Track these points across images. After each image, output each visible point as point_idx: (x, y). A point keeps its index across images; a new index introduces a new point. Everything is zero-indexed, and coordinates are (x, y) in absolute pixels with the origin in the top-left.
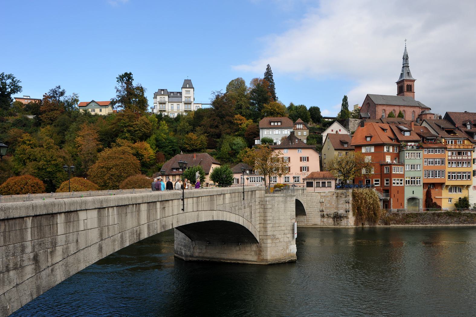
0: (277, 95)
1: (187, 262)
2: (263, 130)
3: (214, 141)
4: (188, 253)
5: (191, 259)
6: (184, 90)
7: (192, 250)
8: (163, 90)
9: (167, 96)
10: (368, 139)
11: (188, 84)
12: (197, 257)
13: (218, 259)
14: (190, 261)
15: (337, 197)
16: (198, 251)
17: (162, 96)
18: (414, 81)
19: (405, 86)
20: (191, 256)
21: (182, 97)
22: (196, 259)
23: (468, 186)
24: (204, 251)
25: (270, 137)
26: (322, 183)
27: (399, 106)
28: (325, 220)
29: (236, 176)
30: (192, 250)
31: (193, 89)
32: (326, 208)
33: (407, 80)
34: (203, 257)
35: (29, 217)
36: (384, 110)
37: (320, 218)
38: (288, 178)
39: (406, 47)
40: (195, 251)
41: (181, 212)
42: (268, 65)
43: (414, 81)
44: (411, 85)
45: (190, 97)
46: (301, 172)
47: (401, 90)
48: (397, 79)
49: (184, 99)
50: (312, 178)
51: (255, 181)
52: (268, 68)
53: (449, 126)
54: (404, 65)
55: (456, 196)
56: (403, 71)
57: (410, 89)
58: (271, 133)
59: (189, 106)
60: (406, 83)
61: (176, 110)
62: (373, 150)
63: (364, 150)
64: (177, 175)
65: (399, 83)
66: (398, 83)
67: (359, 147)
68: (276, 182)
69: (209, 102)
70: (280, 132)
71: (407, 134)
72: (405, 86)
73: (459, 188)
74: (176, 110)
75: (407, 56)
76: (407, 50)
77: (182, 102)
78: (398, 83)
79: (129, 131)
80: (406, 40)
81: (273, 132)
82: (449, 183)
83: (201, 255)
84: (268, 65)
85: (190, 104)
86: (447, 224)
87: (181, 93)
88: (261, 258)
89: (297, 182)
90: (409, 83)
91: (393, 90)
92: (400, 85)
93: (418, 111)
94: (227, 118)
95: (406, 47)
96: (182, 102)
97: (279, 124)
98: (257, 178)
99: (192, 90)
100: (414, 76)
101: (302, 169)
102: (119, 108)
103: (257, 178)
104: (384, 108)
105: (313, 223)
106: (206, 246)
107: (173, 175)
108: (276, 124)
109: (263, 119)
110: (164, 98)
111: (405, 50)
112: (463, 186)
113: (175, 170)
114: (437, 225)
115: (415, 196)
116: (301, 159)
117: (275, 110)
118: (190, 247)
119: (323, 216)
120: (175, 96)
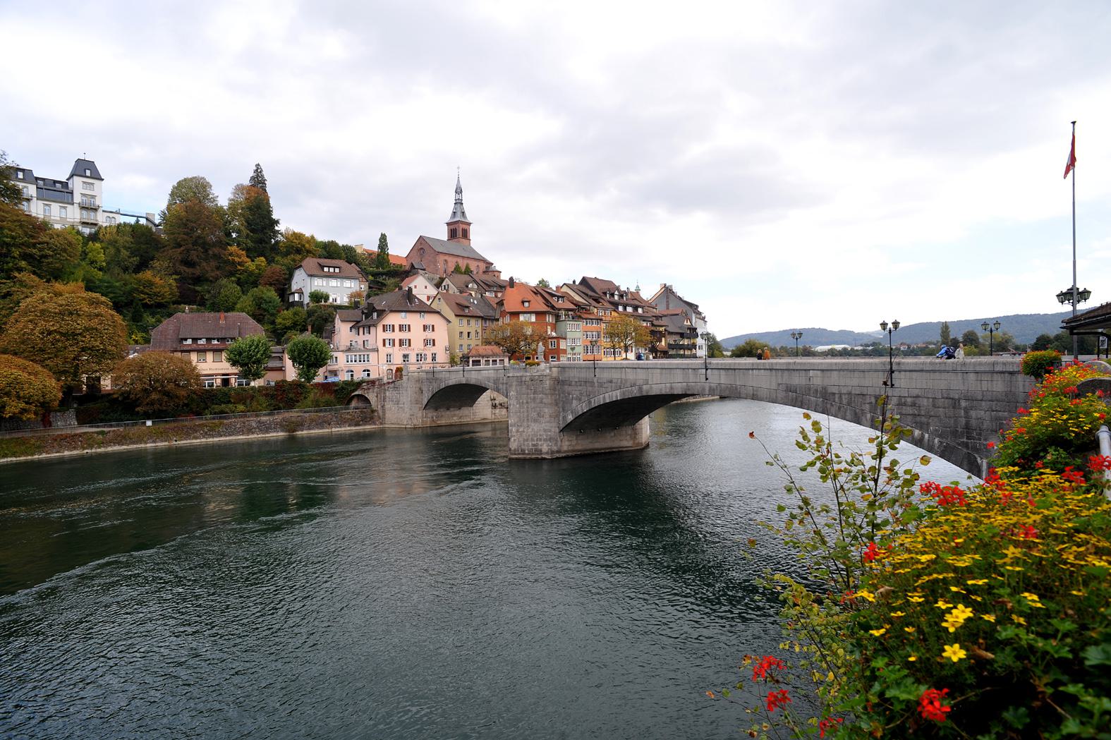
0: (1099, 305)
1: (552, 459)
3: (189, 289)
4: (555, 448)
5: (558, 455)
7: (559, 443)
9: (35, 186)
10: (526, 304)
12: (565, 452)
13: (590, 450)
14: (557, 458)
16: (567, 443)
18: (469, 224)
19: (459, 230)
20: (558, 452)
22: (564, 455)
24: (574, 443)
25: (324, 290)
27: (463, 257)
28: (497, 411)
30: (559, 443)
34: (573, 451)
36: (446, 261)
37: (490, 409)
40: (563, 444)
42: (258, 165)
43: (469, 224)
47: (453, 234)
48: (448, 218)
49: (77, 198)
50: (479, 356)
52: (257, 170)
56: (455, 208)
57: (465, 234)
59: (92, 214)
61: (58, 219)
62: (533, 318)
63: (522, 318)
66: (448, 224)
67: (515, 314)
70: (339, 283)
72: (459, 230)
74: (58, 219)
77: (73, 204)
79: (25, 257)
80: (458, 168)
81: (328, 284)
83: (570, 448)
84: (258, 165)
85: (95, 210)
86: (267, 432)
88: (637, 442)
92: (452, 227)
94: (216, 250)
96: (73, 204)
97: (337, 270)
98: (360, 355)
101: (426, 342)
103: (360, 355)
104: (446, 258)
105: (482, 417)
106: (577, 436)
107: (199, 351)
108: (332, 270)
111: (458, 181)
113: (216, 342)
114: (93, 450)
116: (425, 328)
117: (304, 246)
118: (557, 441)
119: (494, 406)
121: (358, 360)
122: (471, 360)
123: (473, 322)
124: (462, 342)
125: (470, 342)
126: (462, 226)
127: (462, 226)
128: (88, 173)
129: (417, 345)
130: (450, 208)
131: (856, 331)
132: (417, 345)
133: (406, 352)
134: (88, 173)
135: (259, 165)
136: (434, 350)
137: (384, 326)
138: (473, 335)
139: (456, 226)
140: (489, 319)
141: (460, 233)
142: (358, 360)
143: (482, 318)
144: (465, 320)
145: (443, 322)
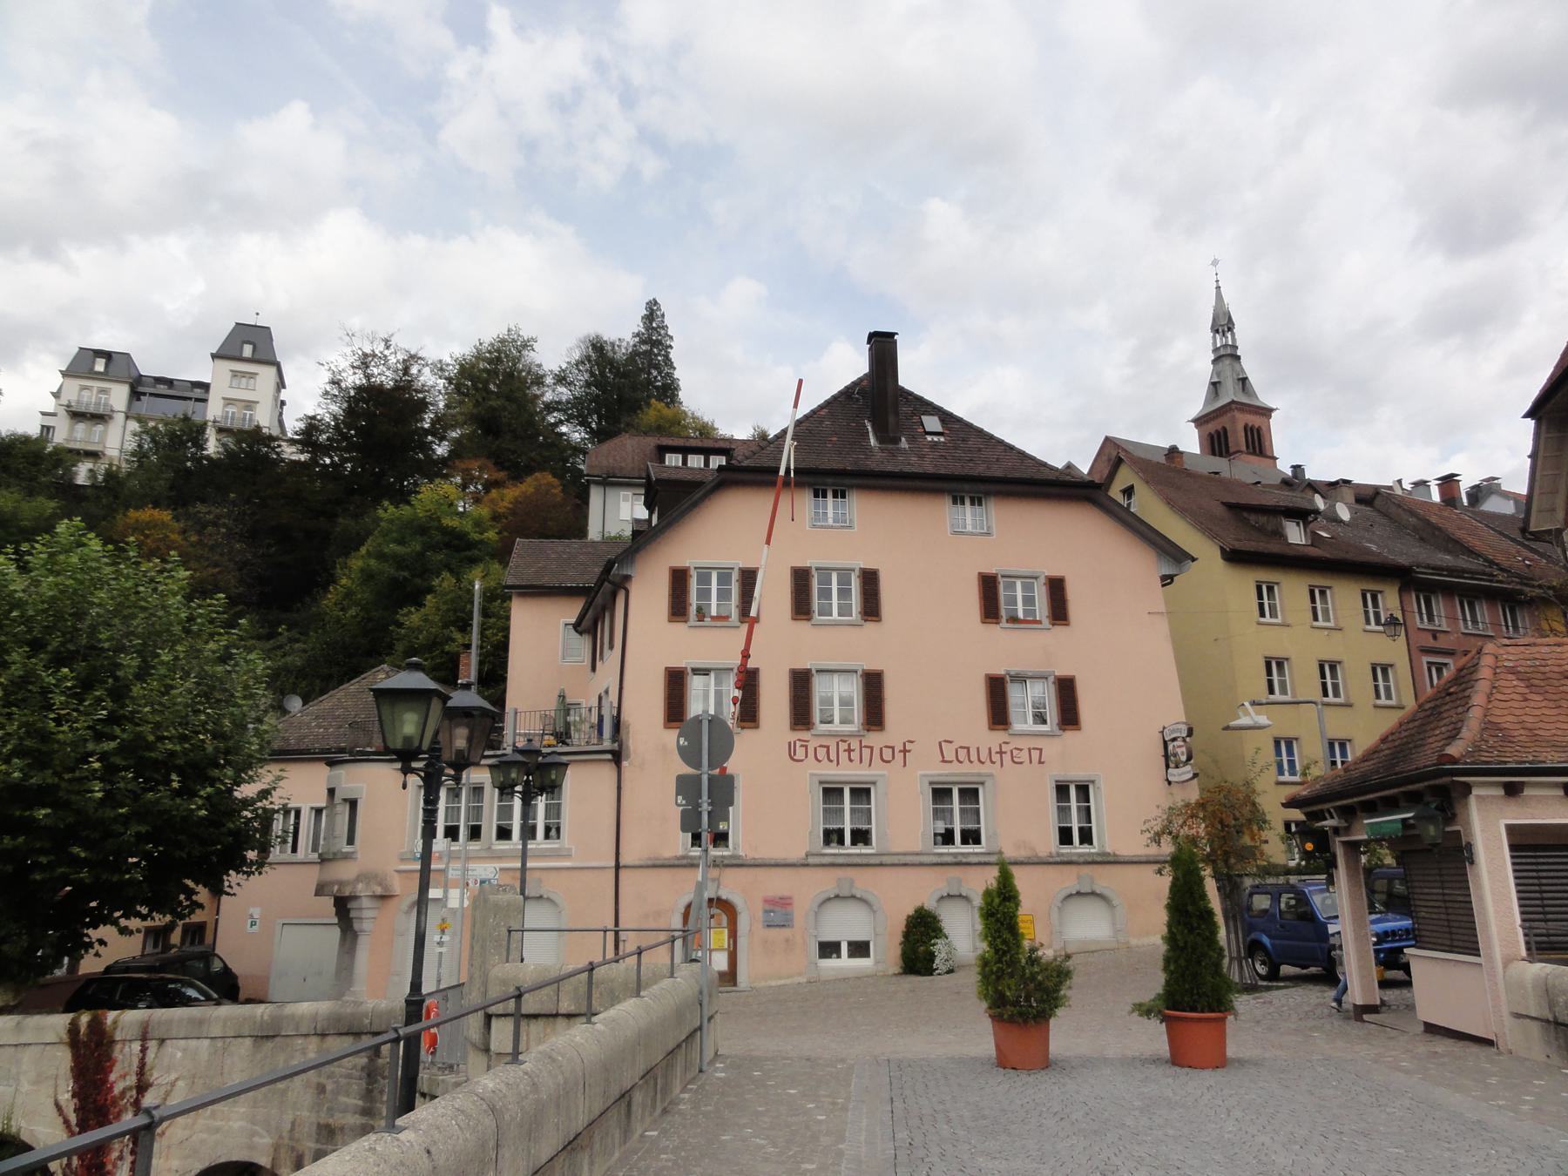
2: (611, 492)
8: (108, 356)
17: (97, 384)
18: (1267, 412)
21: (205, 401)
26: (1071, 842)
29: (300, 787)
31: (272, 370)
38: (861, 793)
39: (1218, 288)
43: (1267, 412)
44: (1259, 430)
45: (250, 405)
46: (1000, 736)
47: (1217, 443)
48: (1197, 407)
51: (475, 833)
54: (1222, 352)
56: (1216, 372)
65: (1207, 422)
68: (1086, 837)
75: (1230, 319)
78: (1199, 421)
80: (1215, 263)
89: (849, 849)
90: (1254, 420)
92: (1212, 427)
95: (1218, 288)
109: (616, 441)
110: (103, 391)
121: (489, 828)
122: (1488, 826)
123: (1345, 597)
124: (1276, 642)
125: (1338, 725)
126: (1243, 419)
127: (1243, 419)
128: (247, 351)
129: (936, 714)
130: (1203, 367)
131: (1166, 918)
132: (936, 714)
133: (848, 772)
134: (247, 351)
135: (656, 303)
136: (1070, 756)
137: (679, 579)
138: (1356, 681)
139: (1224, 421)
140: (1448, 590)
141: (1238, 439)
142: (489, 828)
143: (1404, 577)
144: (1293, 590)
145: (1142, 566)
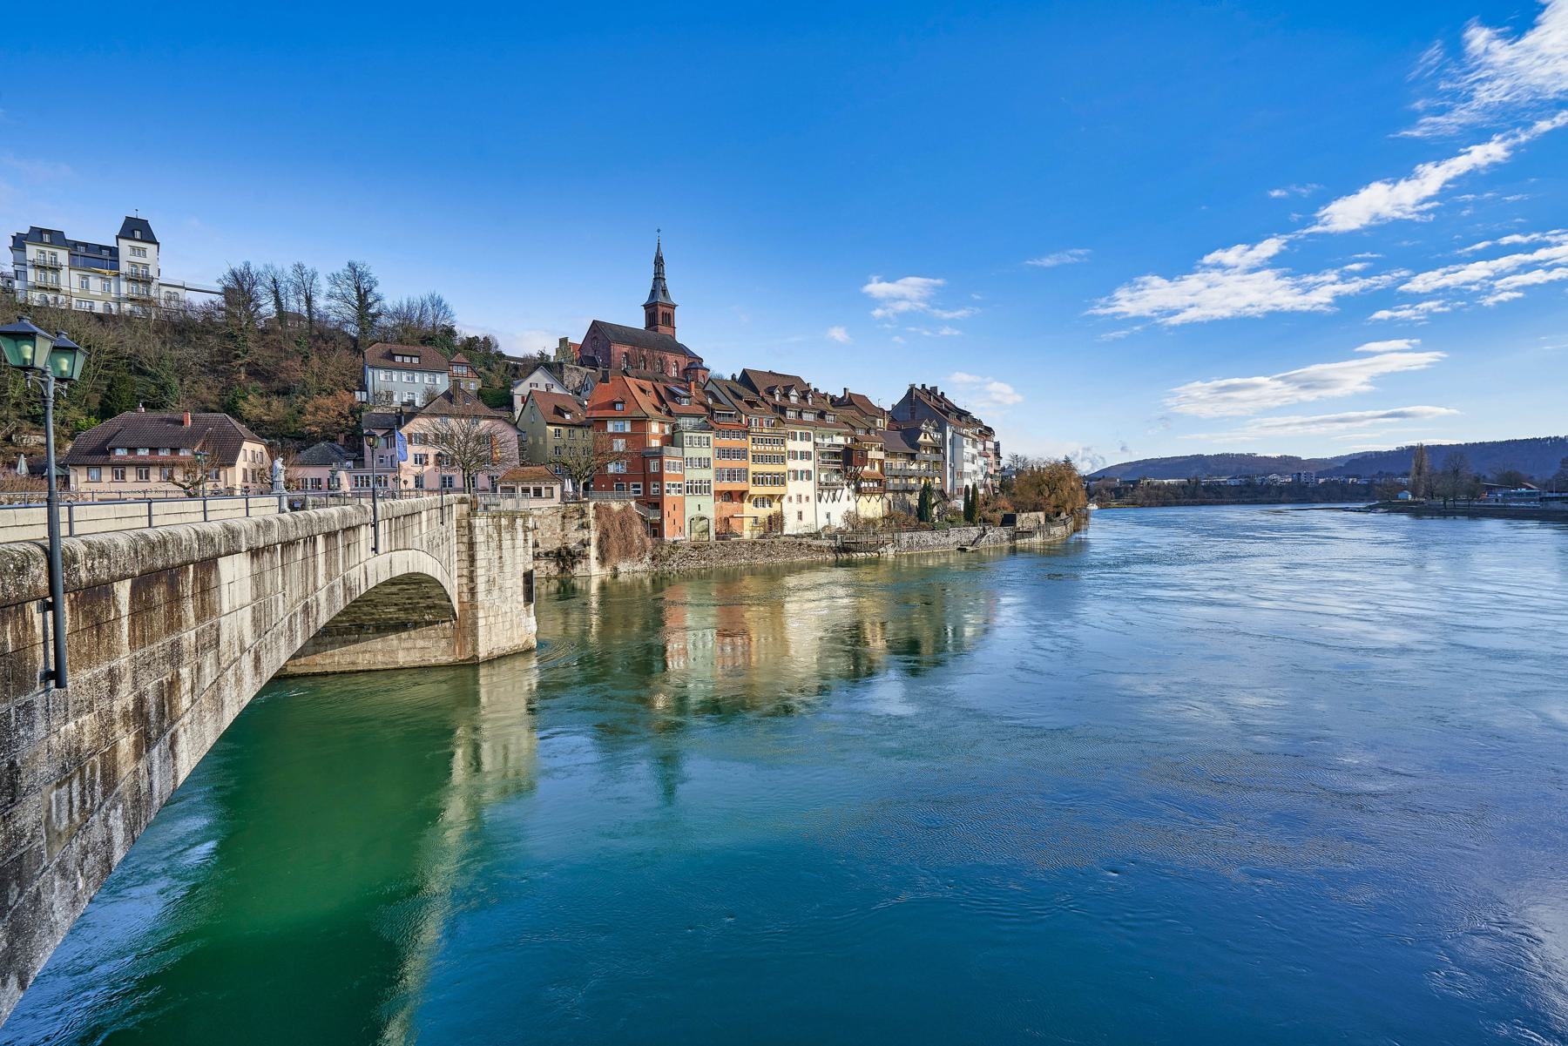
6: (125, 245)
11: (136, 229)
15: (564, 517)
18: (674, 307)
23: (781, 496)
32: (544, 540)
33: (663, 305)
35: (122, 578)
41: (371, 554)
43: (674, 307)
47: (651, 320)
48: (645, 300)
49: (124, 268)
53: (748, 395)
55: (764, 512)
57: (669, 320)
58: (395, 378)
60: (661, 309)
64: (131, 465)
69: (218, 288)
71: (685, 402)
73: (770, 499)
76: (662, 250)
82: (756, 490)
87: (114, 252)
90: (667, 310)
91: (638, 321)
93: (684, 362)
97: (416, 361)
99: (151, 248)
100: (674, 298)
102: (219, 299)
108: (407, 360)
112: (772, 496)
115: (702, 513)
120: (96, 258)
